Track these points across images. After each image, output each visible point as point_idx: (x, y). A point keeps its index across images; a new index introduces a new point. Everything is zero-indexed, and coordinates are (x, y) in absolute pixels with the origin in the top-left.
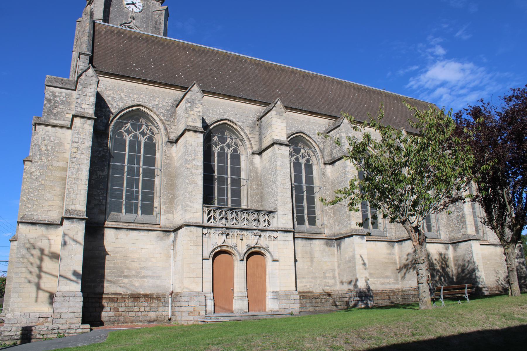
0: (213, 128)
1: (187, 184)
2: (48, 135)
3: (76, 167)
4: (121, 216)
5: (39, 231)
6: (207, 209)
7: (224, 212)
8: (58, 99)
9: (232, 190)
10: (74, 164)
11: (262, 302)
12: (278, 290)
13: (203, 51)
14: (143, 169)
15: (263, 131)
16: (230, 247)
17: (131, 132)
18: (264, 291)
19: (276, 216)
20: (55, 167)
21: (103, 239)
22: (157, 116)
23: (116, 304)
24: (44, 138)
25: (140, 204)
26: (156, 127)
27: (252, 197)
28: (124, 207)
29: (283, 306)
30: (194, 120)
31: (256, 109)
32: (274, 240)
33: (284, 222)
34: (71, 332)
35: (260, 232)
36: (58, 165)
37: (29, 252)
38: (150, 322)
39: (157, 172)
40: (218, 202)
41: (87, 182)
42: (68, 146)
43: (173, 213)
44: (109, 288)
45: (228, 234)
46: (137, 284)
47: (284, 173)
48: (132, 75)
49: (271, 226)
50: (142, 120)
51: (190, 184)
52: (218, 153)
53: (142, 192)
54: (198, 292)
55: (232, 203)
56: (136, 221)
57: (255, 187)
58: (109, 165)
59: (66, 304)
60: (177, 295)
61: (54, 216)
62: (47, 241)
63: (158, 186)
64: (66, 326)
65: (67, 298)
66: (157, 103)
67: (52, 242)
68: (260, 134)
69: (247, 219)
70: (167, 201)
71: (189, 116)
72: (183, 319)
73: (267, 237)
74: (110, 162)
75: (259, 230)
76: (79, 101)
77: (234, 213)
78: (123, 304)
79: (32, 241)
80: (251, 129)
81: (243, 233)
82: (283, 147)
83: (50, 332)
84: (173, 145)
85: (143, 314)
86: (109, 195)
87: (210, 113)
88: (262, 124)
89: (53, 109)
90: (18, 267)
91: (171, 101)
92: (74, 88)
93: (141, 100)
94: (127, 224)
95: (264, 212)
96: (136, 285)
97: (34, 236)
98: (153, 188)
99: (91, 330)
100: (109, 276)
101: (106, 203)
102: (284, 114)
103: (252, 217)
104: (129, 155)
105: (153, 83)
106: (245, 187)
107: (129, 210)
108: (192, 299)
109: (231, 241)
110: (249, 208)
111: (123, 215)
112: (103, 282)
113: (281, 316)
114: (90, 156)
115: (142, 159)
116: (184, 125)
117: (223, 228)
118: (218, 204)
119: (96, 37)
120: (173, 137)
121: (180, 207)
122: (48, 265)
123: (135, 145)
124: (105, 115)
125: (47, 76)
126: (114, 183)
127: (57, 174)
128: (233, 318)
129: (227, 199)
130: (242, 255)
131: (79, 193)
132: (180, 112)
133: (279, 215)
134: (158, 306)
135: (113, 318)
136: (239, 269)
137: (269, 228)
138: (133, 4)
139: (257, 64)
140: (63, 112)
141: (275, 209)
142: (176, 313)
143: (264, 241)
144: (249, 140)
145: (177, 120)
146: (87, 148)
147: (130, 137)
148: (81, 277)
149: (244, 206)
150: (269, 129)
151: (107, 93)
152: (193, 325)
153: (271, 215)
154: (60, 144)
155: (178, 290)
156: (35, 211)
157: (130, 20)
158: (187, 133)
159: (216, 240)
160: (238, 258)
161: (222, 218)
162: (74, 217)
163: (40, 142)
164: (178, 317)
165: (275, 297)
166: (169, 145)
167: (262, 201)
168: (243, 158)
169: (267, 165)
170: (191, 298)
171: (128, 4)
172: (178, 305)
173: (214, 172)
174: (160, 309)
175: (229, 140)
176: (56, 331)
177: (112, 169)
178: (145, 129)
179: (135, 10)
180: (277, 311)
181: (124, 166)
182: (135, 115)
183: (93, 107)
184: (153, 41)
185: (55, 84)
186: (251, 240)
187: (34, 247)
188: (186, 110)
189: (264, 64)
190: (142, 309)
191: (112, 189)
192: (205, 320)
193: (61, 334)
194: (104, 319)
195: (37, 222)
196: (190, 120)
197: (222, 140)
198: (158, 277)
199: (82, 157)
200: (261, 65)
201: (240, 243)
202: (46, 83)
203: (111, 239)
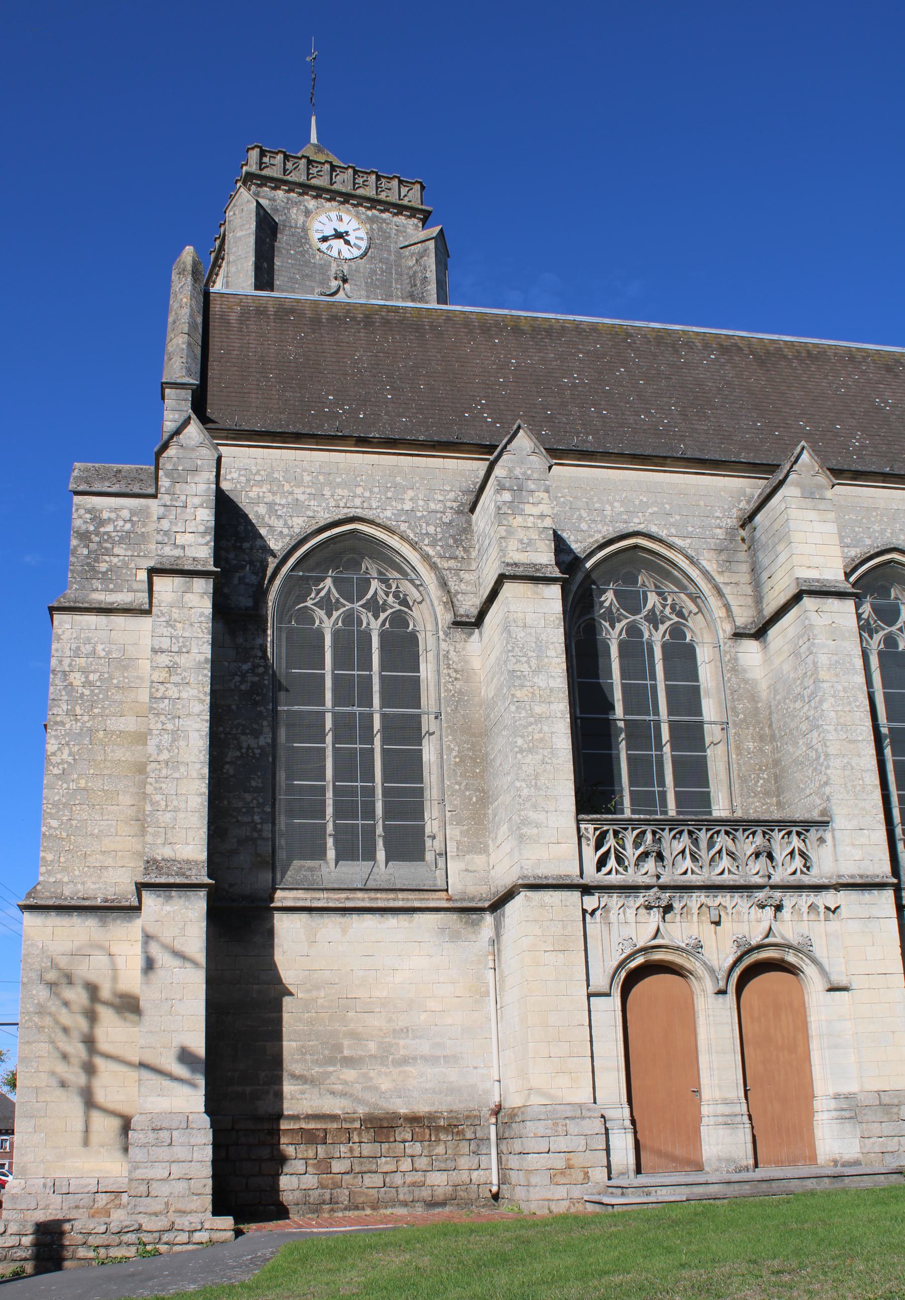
0: (596, 565)
1: (521, 751)
2: (88, 641)
3: (169, 726)
4: (324, 870)
5: (82, 929)
6: (591, 827)
7: (649, 836)
8: (109, 528)
9: (675, 761)
10: (163, 718)
11: (801, 1130)
12: (852, 1087)
13: (546, 330)
14: (384, 716)
15: (764, 559)
16: (678, 949)
17: (338, 605)
18: (805, 1094)
19: (828, 836)
20: (113, 732)
21: (272, 946)
22: (414, 545)
23: (321, 1149)
24: (78, 648)
25: (379, 830)
26: (412, 581)
27: (744, 780)
28: (330, 842)
29: (876, 1145)
30: (528, 544)
31: (732, 490)
32: (827, 920)
33: (857, 854)
34: (178, 1240)
35: (777, 894)
36: (122, 727)
37: (57, 995)
38: (432, 1204)
39: (428, 723)
40: (632, 804)
41: (206, 771)
42: (145, 666)
43: (485, 850)
44: (298, 1099)
45: (668, 909)
46: (385, 1085)
47: (845, 690)
48: (327, 429)
49: (814, 871)
50: (369, 567)
51: (530, 751)
52: (622, 645)
53: (386, 792)
54: (580, 1106)
55: (679, 803)
56: (371, 884)
57: (751, 746)
58: (275, 713)
59: (163, 1153)
60: (513, 1115)
61: (119, 882)
62: (105, 959)
63: (435, 769)
64: (161, 1223)
65: (164, 1135)
66: (408, 506)
67: (120, 962)
68: (755, 570)
69: (731, 854)
70: (466, 813)
71: (510, 532)
72: (532, 1196)
73: (805, 909)
74: (275, 703)
75: (773, 887)
76: (165, 525)
77: (686, 834)
78: (343, 1148)
79: (63, 962)
80: (723, 557)
81: (719, 900)
82: (833, 604)
83: (116, 1239)
84: (471, 634)
85: (409, 1179)
86: (281, 807)
87: (580, 518)
88: (757, 534)
89: (97, 560)
90: (28, 1042)
91: (452, 495)
92: (151, 491)
93: (358, 502)
94: (343, 895)
95: (786, 825)
96: (383, 1087)
97: (67, 946)
98: (418, 776)
99: (238, 1233)
100: (297, 1061)
101: (273, 832)
102: (829, 494)
103: (748, 845)
104: (336, 678)
105: (392, 444)
106: (721, 749)
107: (345, 853)
108: (560, 1129)
109: (680, 931)
110: (739, 814)
111: (331, 868)
112: (278, 1080)
113: (867, 1182)
114: (208, 689)
115: (376, 687)
116: (497, 563)
117: (648, 887)
118: (633, 812)
119: (213, 332)
120: (469, 605)
121: (504, 829)
122: (113, 1031)
123: (352, 645)
124: (251, 563)
125: (77, 464)
126: (291, 769)
127: (121, 754)
128: (700, 1190)
129: (663, 794)
130: (722, 975)
131: (183, 806)
132: (482, 525)
133: (838, 834)
134: (457, 1155)
135: (314, 1195)
136: (715, 1023)
137: (806, 880)
138: (339, 235)
139: (728, 349)
140: (126, 565)
141: (824, 812)
142: (514, 1177)
143: (793, 924)
144: (720, 593)
145: (473, 556)
146: (199, 667)
147: (336, 622)
148: (202, 1067)
149: (720, 809)
150: (780, 547)
151: (251, 494)
152: (564, 1217)
153: (813, 834)
154: (125, 663)
155: (513, 1101)
156: (65, 870)
157: (334, 284)
158: (509, 589)
159: (629, 928)
160: (710, 986)
161: (646, 854)
162: (171, 880)
163: (67, 661)
164: (518, 1188)
165: (846, 1114)
166: (459, 634)
167: (779, 792)
168: (704, 655)
169: (786, 668)
170: (556, 1124)
171: (325, 239)
172: (518, 1150)
173: (612, 708)
174: (464, 1162)
175: (653, 599)
176: (131, 1238)
177: (288, 726)
178: (380, 592)
179: (347, 252)
180: (857, 1163)
181: (322, 715)
182: (345, 550)
183: (209, 538)
184: (386, 322)
185: (97, 487)
186: (748, 922)
187: (69, 979)
188: (499, 513)
189: (749, 345)
190: (406, 1165)
191: (291, 789)
192: (606, 1200)
193: (149, 1248)
194: (287, 1197)
195: (73, 903)
196: (513, 545)
197: (631, 601)
198: (452, 1059)
199: (184, 695)
200: (740, 349)
201: (712, 937)
202: (72, 486)
203: (300, 946)
